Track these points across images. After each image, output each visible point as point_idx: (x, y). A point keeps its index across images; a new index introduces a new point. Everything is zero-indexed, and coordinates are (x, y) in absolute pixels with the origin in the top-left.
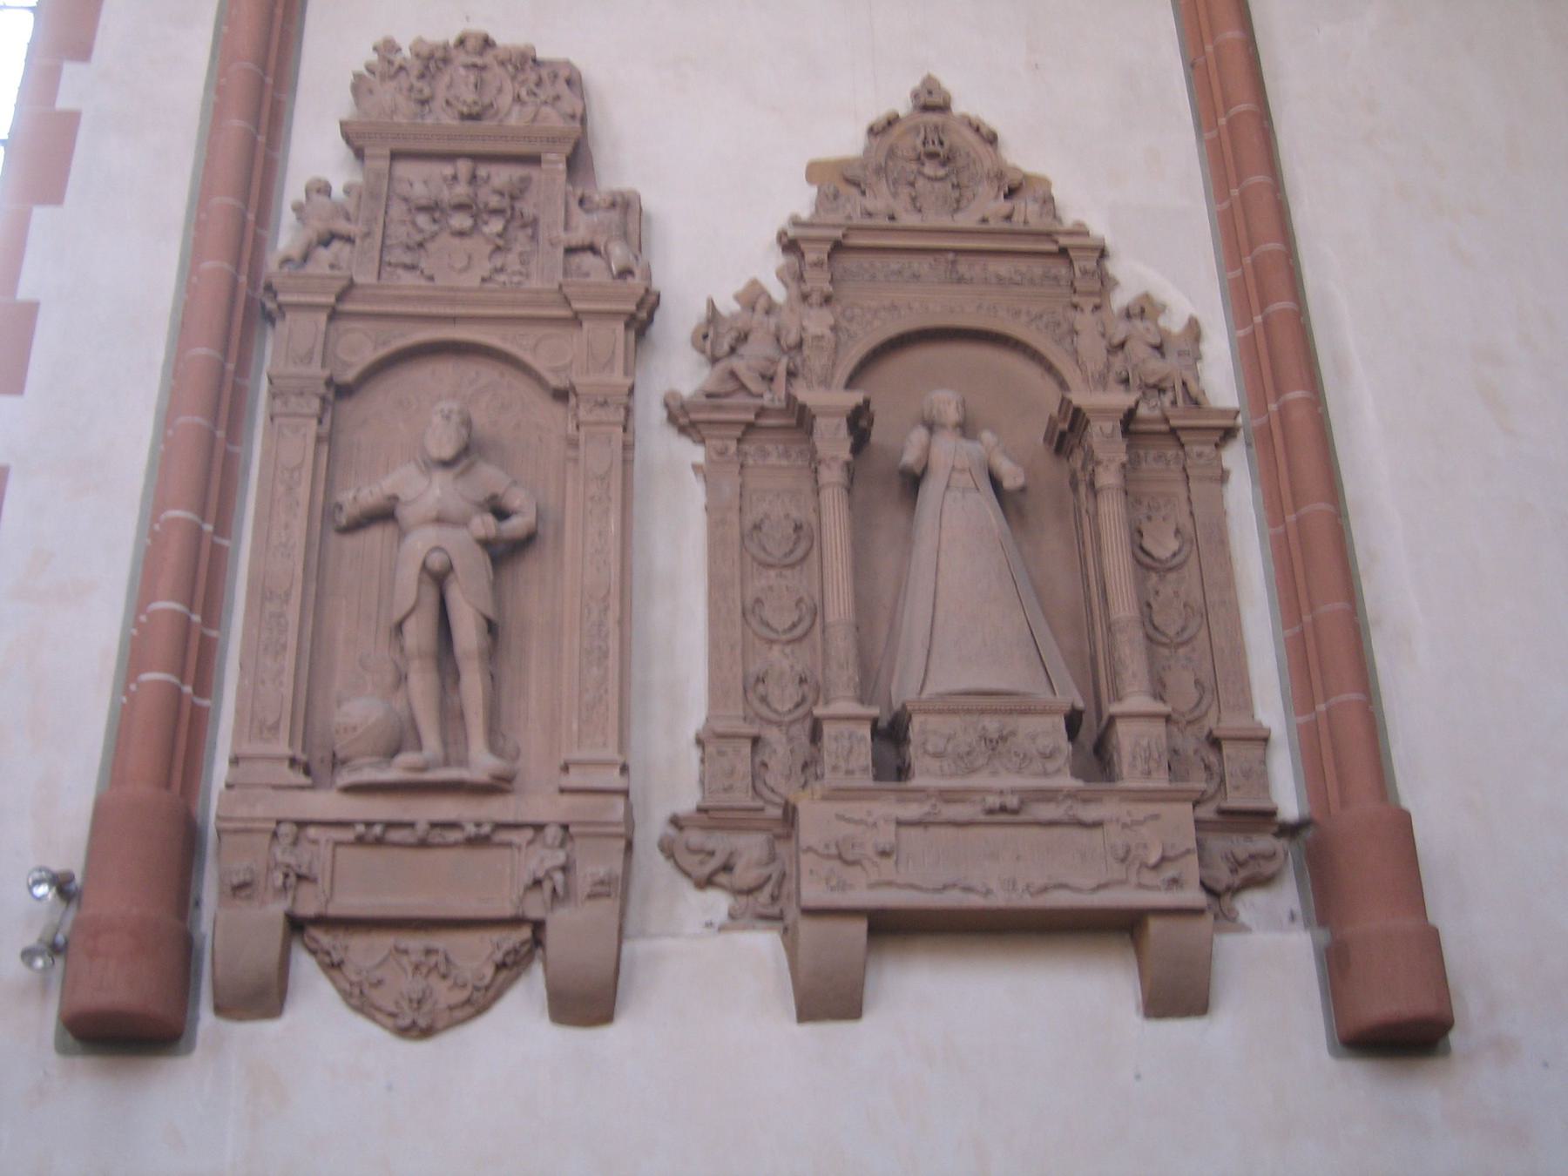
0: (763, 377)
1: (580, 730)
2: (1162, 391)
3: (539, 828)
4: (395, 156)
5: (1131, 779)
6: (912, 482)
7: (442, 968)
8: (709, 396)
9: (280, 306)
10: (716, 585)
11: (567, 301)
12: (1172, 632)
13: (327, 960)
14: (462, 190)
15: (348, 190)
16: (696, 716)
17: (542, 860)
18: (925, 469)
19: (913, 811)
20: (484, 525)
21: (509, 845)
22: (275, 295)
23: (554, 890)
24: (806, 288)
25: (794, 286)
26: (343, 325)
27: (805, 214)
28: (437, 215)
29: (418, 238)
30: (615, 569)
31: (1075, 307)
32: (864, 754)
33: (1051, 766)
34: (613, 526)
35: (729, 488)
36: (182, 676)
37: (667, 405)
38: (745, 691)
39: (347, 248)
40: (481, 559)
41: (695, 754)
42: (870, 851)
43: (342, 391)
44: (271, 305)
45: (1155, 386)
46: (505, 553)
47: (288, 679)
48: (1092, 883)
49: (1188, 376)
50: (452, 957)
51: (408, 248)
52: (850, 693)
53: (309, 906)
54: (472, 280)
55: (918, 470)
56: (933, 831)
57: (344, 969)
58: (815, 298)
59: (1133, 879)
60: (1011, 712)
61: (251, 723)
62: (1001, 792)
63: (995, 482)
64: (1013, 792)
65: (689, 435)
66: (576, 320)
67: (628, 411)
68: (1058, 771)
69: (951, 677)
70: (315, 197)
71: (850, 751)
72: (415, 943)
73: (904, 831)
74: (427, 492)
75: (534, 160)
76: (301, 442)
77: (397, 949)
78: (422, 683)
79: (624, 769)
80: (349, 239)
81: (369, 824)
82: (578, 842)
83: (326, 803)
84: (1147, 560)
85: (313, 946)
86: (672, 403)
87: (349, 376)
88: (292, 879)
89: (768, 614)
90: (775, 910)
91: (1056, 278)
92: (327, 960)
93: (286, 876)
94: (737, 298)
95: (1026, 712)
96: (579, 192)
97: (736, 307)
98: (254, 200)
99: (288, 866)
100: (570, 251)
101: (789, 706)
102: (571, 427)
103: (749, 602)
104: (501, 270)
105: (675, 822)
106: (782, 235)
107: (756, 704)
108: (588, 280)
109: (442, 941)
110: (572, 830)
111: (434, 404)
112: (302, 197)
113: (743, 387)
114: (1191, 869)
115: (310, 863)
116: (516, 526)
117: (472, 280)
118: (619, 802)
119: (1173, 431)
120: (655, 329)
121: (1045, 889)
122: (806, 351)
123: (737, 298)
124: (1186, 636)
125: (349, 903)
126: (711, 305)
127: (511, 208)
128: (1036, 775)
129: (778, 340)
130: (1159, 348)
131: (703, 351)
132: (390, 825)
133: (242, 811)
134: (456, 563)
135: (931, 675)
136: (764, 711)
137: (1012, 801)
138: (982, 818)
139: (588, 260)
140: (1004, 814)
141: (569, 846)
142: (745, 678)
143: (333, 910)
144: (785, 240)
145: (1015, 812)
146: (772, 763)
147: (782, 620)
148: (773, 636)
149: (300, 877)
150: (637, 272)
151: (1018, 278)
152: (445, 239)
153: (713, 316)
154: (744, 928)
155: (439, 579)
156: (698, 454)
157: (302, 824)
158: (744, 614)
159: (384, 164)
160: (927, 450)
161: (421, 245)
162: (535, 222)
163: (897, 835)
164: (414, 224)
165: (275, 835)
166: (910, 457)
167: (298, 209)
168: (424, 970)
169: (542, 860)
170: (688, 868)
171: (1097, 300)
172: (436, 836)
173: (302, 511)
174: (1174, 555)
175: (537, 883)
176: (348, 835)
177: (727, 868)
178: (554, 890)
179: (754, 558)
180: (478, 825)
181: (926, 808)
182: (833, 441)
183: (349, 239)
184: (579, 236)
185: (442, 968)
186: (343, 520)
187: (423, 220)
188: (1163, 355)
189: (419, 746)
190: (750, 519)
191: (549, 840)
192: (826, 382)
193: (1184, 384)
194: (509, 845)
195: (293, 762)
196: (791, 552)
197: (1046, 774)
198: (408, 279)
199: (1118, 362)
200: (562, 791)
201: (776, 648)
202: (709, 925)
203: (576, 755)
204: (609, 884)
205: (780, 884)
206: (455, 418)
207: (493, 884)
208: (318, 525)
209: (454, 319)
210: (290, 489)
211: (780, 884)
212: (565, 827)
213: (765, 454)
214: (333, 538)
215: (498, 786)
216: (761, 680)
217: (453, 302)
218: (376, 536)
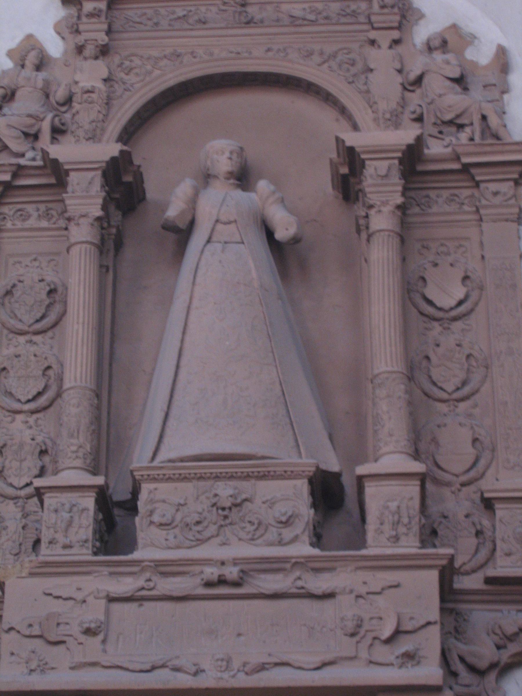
0: (26, 135)
2: (461, 127)
5: (376, 545)
6: (181, 234)
12: (450, 388)
18: (192, 223)
19: (126, 585)
31: (373, 42)
32: (85, 526)
33: (288, 534)
42: (76, 630)
45: (451, 122)
48: (317, 660)
49: (489, 110)
52: (78, 463)
55: (182, 225)
56: (148, 605)
58: (89, 50)
59: (364, 654)
60: (247, 477)
62: (223, 563)
63: (269, 234)
64: (235, 562)
68: (295, 539)
69: (186, 441)
71: (70, 524)
73: (116, 607)
84: (430, 310)
91: (354, 14)
94: (10, 54)
95: (263, 477)
114: (431, 642)
119: (466, 169)
121: (262, 667)
122: (76, 106)
124: (467, 390)
128: (271, 544)
130: (460, 81)
135: (166, 440)
137: (232, 572)
138: (202, 591)
140: (223, 586)
145: (237, 584)
148: (17, 406)
151: (312, 17)
160: (193, 202)
163: (107, 613)
166: (173, 211)
171: (396, 34)
174: (460, 303)
181: (141, 582)
182: (86, 197)
188: (466, 89)
192: (93, 137)
193: (484, 118)
196: (43, 317)
197: (281, 543)
199: (415, 99)
201: (20, 418)
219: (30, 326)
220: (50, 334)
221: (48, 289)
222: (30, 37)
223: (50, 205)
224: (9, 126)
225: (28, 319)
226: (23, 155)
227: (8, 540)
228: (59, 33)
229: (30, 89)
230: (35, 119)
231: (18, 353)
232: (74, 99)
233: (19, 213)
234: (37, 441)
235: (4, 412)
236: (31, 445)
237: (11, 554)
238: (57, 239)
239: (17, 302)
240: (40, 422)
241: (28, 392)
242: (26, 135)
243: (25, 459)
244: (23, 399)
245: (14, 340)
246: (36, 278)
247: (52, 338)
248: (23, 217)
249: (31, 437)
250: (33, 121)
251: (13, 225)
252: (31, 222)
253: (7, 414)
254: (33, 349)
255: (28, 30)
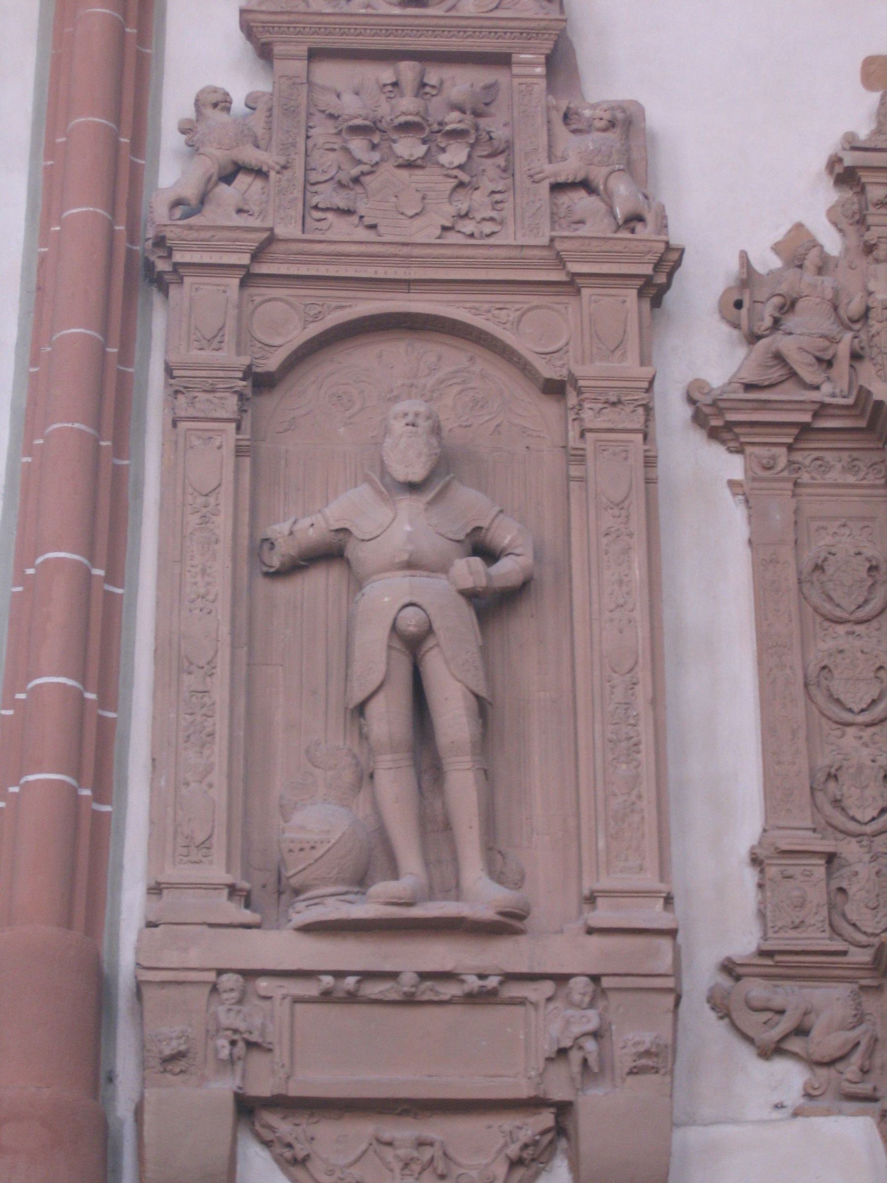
0: (819, 360)
1: (608, 847)
3: (561, 979)
4: (314, 55)
7: (441, 1167)
8: (749, 387)
9: (176, 266)
10: (768, 649)
11: (560, 261)
13: (288, 1154)
14: (407, 105)
15: (251, 104)
16: (748, 828)
17: (568, 1023)
20: (469, 571)
21: (522, 1002)
22: (170, 251)
23: (585, 1061)
24: (871, 236)
25: (851, 230)
26: (259, 292)
27: (864, 132)
28: (376, 139)
29: (355, 171)
30: (642, 632)
34: (638, 572)
35: (779, 516)
36: (78, 774)
37: (691, 401)
38: (812, 789)
39: (258, 184)
40: (467, 613)
41: (750, 876)
43: (262, 382)
44: (162, 266)
46: (492, 606)
47: (218, 777)
50: (451, 1151)
51: (341, 185)
53: (262, 1088)
54: (424, 231)
57: (309, 1164)
61: (168, 835)
65: (723, 442)
66: (572, 285)
67: (648, 409)
70: (208, 111)
72: (404, 1131)
74: (392, 528)
75: (502, 60)
76: (214, 459)
77: (380, 1142)
78: (394, 784)
79: (668, 900)
80: (260, 173)
81: (339, 975)
82: (614, 998)
83: (279, 947)
85: (268, 1135)
86: (696, 396)
87: (272, 363)
88: (241, 1047)
89: (838, 687)
90: (865, 1088)
92: (288, 1154)
93: (233, 1043)
94: (777, 248)
96: (563, 105)
97: (776, 263)
98: (128, 116)
99: (236, 1031)
100: (557, 188)
101: (871, 813)
102: (573, 433)
103: (813, 670)
104: (466, 216)
105: (729, 968)
106: (834, 162)
107: (828, 809)
108: (583, 231)
109: (436, 1129)
110: (606, 982)
111: (394, 401)
112: (190, 112)
113: (793, 374)
115: (264, 1026)
116: (507, 570)
117: (424, 231)
118: (665, 943)
120: (670, 297)
122: (875, 326)
123: (777, 248)
125: (316, 1079)
126: (744, 259)
127: (473, 127)
129: (836, 308)
131: (736, 326)
132: (367, 976)
133: (171, 958)
134: (436, 625)
136: (840, 820)
139: (580, 200)
141: (601, 1004)
142: (812, 777)
143: (294, 1090)
144: (839, 169)
146: (852, 890)
147: (857, 695)
148: (847, 717)
149: (251, 1045)
150: (650, 217)
152: (388, 171)
153: (748, 277)
154: (828, 1113)
155: (413, 645)
156: (734, 467)
157: (250, 975)
158: (806, 685)
159: (300, 66)
161: (356, 180)
162: (507, 149)
164: (347, 150)
165: (214, 989)
167: (186, 129)
168: (416, 1168)
169: (568, 1023)
170: (751, 1033)
172: (427, 991)
173: (223, 550)
175: (563, 1052)
176: (311, 989)
177: (801, 1031)
178: (585, 1061)
179: (816, 610)
180: (482, 976)
183: (260, 173)
184: (568, 170)
185: (441, 1167)
186: (276, 562)
187: (357, 145)
189: (394, 873)
190: (809, 557)
191: (577, 997)
194: (522, 1002)
195: (233, 890)
196: (866, 601)
198: (341, 229)
200: (591, 931)
201: (851, 731)
202: (779, 1106)
203: (605, 883)
204: (657, 1055)
205: (870, 1053)
206: (424, 425)
207: (503, 1054)
208: (244, 571)
209: (407, 284)
210: (205, 520)
211: (870, 1053)
212: (595, 979)
213: (825, 468)
214: (262, 584)
215: (507, 925)
216: (832, 777)
217: (407, 261)
218: (319, 582)
219: (852, 613)
220: (874, 624)
221: (867, 565)
222: (799, 227)
223: (855, 454)
224: (801, 349)
225: (849, 604)
226: (817, 388)
227: (861, 889)
228: (835, 224)
229: (818, 300)
230: (828, 339)
231: (841, 648)
232: (872, 314)
233: (818, 463)
234: (879, 763)
235: (830, 723)
236: (872, 768)
237: (867, 907)
238: (868, 499)
239: (830, 580)
240: (877, 738)
241: (861, 699)
242: (819, 360)
243: (867, 786)
244: (857, 709)
245: (831, 629)
246: (852, 551)
247: (878, 629)
248: (823, 469)
249: (872, 757)
250: (827, 343)
251: (813, 478)
252: (833, 476)
253: (835, 726)
254: (858, 643)
255: (797, 219)
